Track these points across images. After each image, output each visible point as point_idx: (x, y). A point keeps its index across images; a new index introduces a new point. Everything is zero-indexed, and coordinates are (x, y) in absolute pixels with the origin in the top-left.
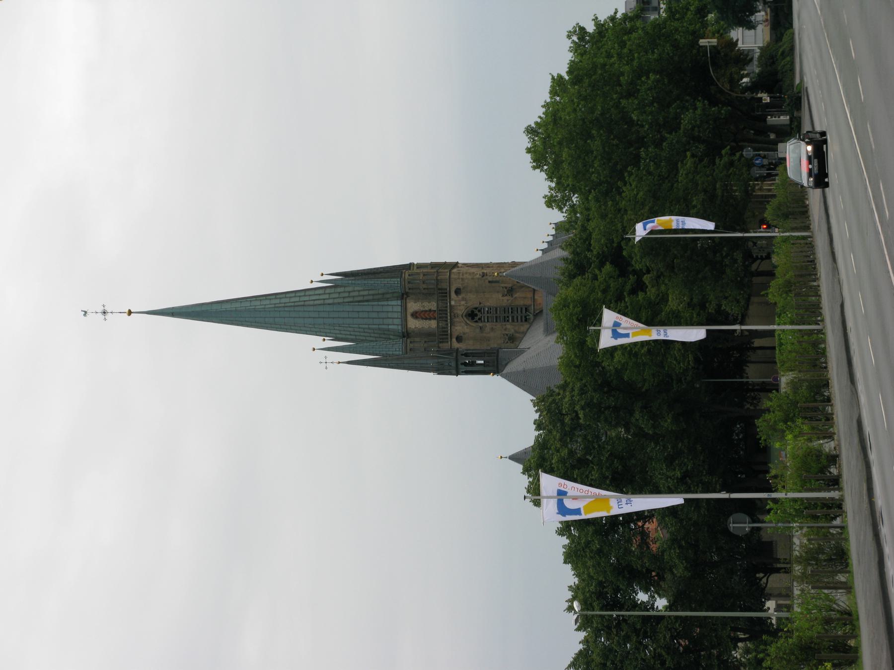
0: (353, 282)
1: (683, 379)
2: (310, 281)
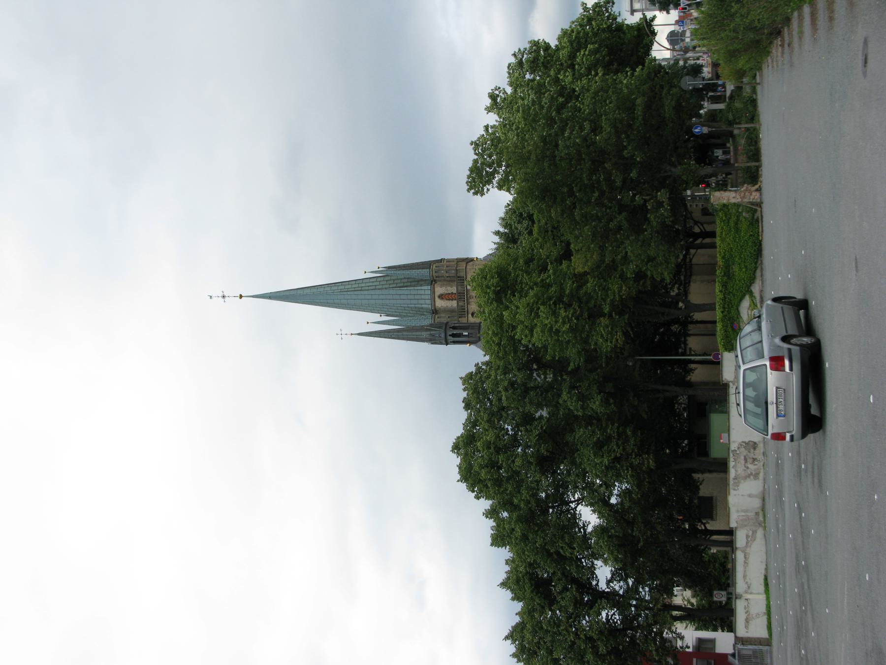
0: (395, 272)
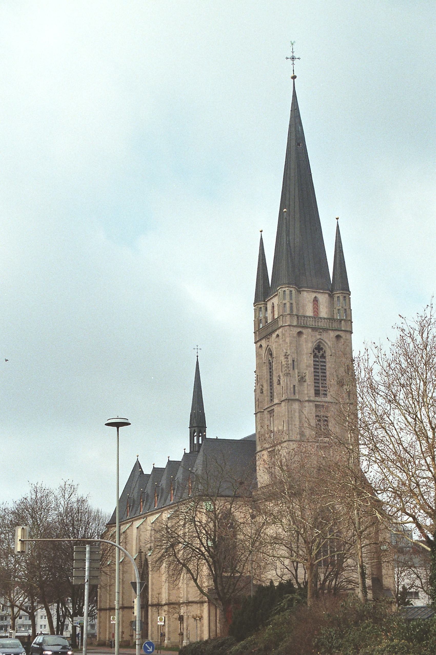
1: (91, 524)
2: (261, 230)
